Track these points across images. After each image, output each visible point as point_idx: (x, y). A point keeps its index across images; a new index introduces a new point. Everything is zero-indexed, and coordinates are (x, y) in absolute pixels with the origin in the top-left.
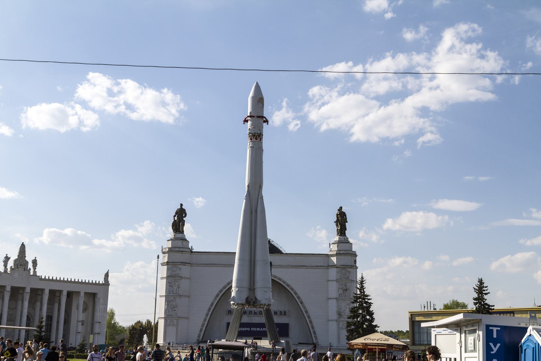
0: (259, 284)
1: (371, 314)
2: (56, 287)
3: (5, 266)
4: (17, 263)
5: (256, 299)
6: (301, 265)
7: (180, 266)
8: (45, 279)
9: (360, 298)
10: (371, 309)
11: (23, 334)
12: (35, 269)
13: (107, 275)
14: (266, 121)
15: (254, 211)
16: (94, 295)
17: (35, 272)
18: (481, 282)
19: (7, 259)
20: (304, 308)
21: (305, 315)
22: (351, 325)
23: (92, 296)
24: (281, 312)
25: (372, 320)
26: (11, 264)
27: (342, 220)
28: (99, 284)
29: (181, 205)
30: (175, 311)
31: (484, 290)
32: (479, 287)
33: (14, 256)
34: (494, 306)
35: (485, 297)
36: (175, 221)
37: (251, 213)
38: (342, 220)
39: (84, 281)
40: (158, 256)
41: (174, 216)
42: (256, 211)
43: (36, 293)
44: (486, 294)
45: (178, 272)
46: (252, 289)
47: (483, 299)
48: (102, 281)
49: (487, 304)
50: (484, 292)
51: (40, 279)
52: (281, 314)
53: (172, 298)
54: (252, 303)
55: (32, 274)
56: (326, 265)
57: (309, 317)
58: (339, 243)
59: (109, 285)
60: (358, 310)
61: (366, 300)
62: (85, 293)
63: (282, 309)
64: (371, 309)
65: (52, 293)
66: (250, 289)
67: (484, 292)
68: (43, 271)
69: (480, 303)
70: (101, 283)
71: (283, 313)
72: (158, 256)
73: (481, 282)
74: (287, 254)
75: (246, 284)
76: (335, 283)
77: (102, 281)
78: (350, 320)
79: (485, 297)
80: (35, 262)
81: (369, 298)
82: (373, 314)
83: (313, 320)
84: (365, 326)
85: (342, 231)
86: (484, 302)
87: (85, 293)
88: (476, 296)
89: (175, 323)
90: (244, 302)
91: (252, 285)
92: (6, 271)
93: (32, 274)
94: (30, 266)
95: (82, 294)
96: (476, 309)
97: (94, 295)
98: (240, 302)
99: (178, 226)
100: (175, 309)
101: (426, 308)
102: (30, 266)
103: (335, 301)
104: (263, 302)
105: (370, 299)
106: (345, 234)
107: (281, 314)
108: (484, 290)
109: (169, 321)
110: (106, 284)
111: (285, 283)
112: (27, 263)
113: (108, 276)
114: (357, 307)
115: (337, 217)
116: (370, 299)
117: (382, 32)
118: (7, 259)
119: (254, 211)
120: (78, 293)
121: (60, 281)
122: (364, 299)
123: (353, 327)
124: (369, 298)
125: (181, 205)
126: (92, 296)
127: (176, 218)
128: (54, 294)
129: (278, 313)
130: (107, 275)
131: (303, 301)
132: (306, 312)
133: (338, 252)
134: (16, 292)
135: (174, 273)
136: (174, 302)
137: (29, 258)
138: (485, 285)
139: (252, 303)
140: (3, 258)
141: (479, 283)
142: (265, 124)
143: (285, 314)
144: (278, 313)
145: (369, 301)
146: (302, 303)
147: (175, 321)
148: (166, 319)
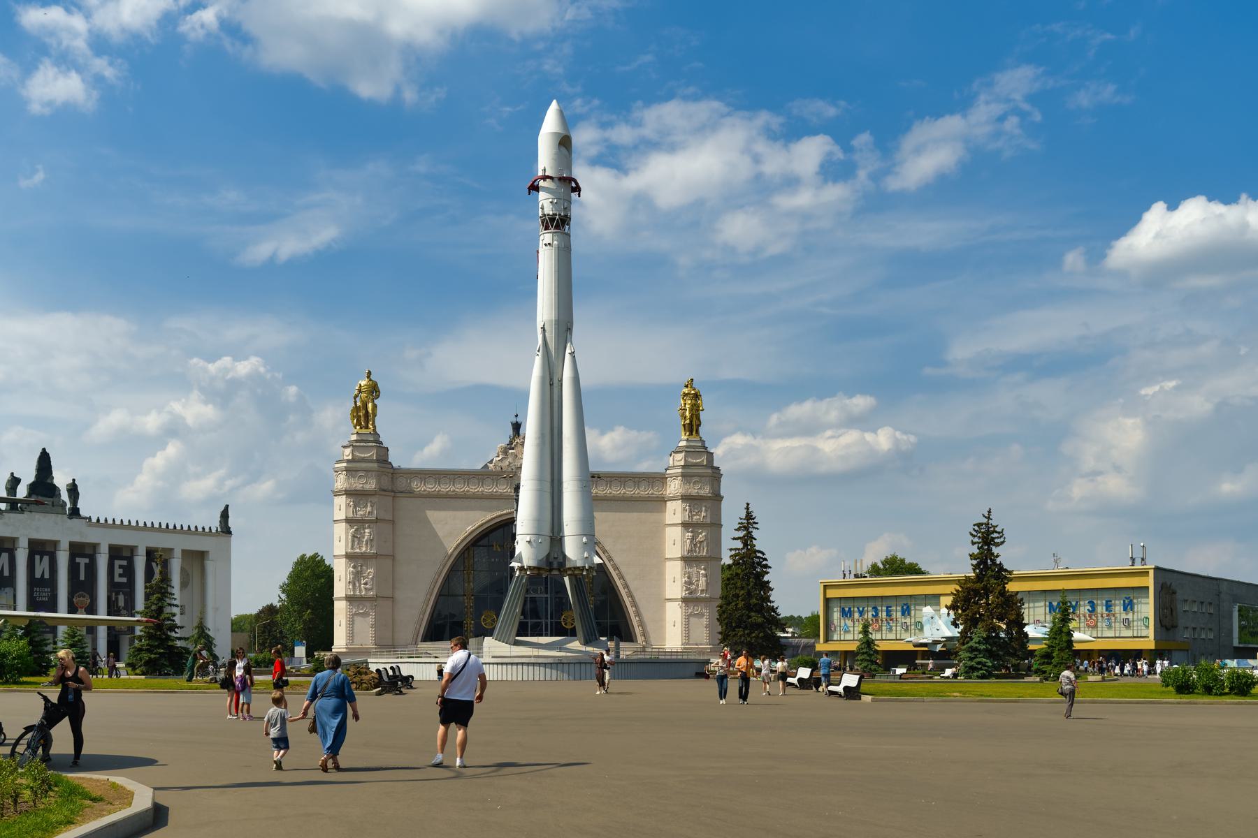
11: (102, 632)
13: (225, 515)
14: (577, 189)
16: (201, 556)
19: (14, 482)
23: (197, 558)
33: (28, 475)
37: (551, 385)
44: (997, 545)
46: (556, 539)
58: (688, 451)
62: (184, 551)
65: (116, 552)
66: (552, 539)
77: (215, 524)
79: (995, 550)
80: (73, 490)
85: (693, 427)
87: (184, 551)
94: (65, 496)
95: (178, 554)
99: (363, 416)
101: (1138, 561)
102: (65, 496)
110: (226, 530)
117: (40, 177)
130: (225, 515)
137: (61, 480)
142: (574, 195)
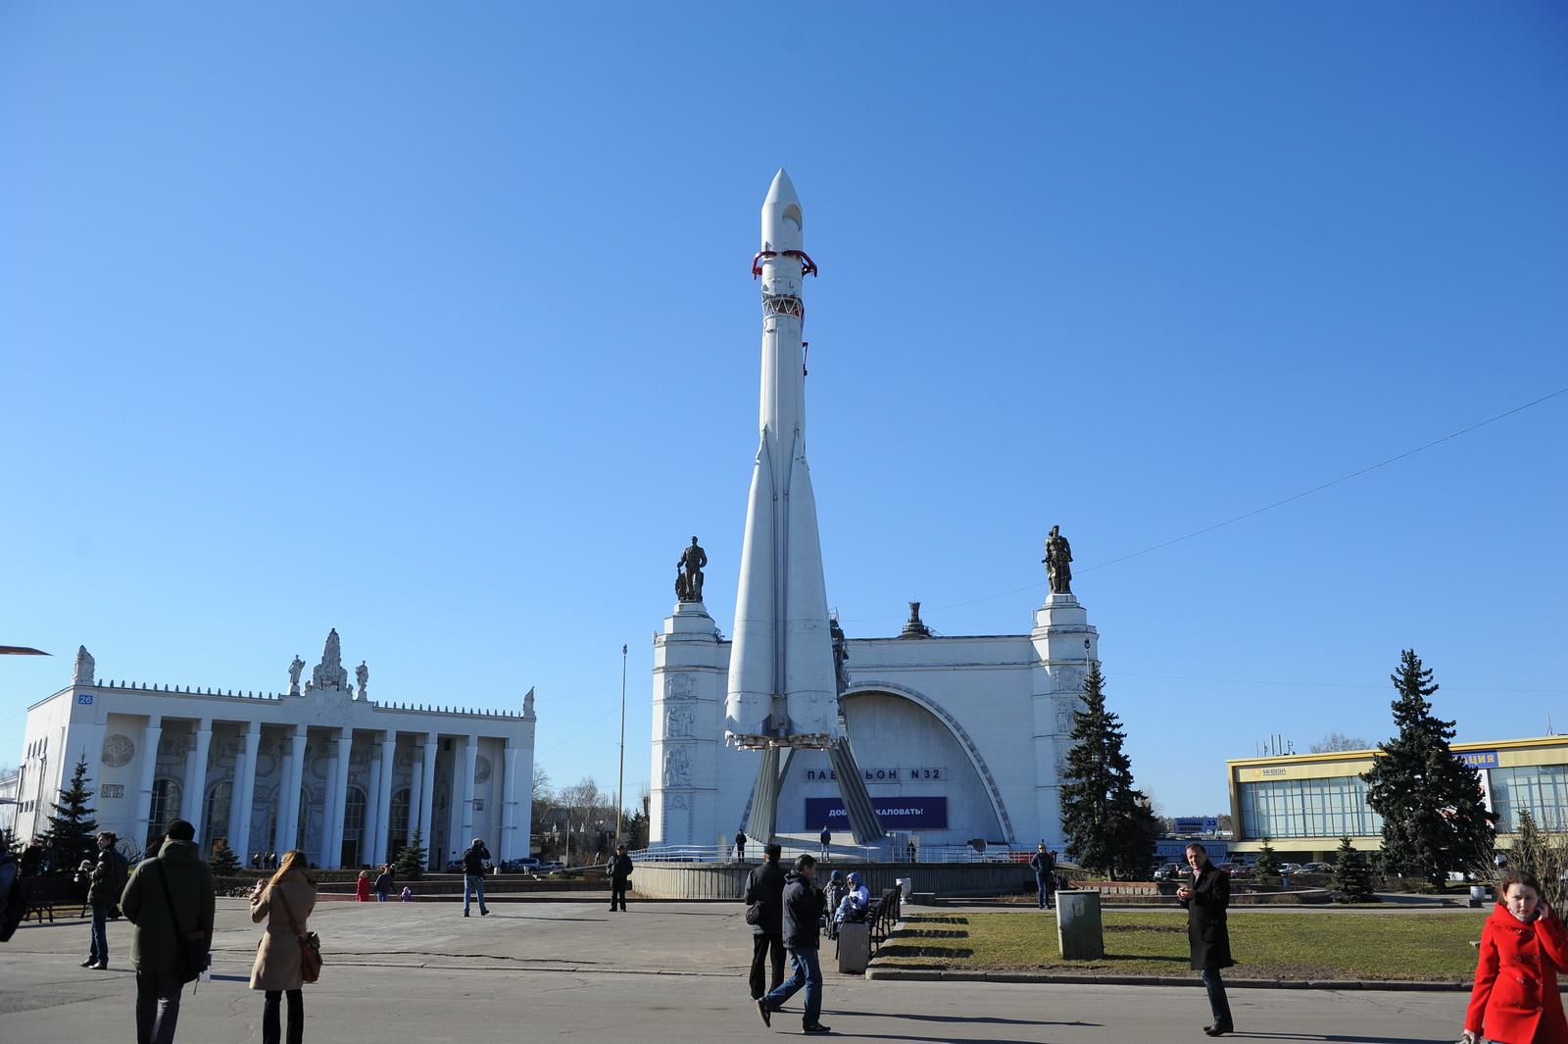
0: (795, 682)
1: (1122, 763)
2: (412, 726)
3: (295, 683)
4: (322, 673)
5: (790, 722)
6: (967, 661)
7: (692, 675)
8: (386, 709)
9: (1092, 724)
10: (1122, 752)
12: (363, 686)
15: (780, 495)
16: (502, 743)
17: (362, 692)
18: (1411, 659)
19: (298, 665)
20: (980, 760)
21: (982, 776)
22: (1072, 793)
23: (498, 744)
24: (927, 772)
25: (1127, 779)
26: (307, 676)
27: (1059, 556)
28: (512, 718)
29: (695, 540)
30: (684, 774)
31: (1423, 684)
32: (1406, 674)
33: (314, 658)
34: (1453, 723)
35: (1426, 699)
36: (681, 576)
38: (1059, 556)
39: (442, 710)
40: (625, 647)
41: (680, 565)
42: (786, 494)
43: (367, 742)
44: (1427, 692)
45: (689, 687)
47: (1422, 707)
48: (518, 710)
49: (1432, 721)
50: (1421, 688)
51: (375, 707)
52: (928, 777)
53: (678, 747)
54: (782, 734)
55: (355, 696)
56: (1025, 660)
57: (991, 781)
59: (534, 719)
60: (1089, 754)
61: (1109, 729)
63: (931, 763)
64: (1122, 752)
67: (1421, 688)
68: (383, 691)
69: (1415, 721)
70: (516, 715)
71: (932, 775)
72: (625, 647)
73: (1411, 659)
74: (942, 638)
75: (764, 684)
76: (1048, 699)
77: (518, 710)
78: (1070, 782)
79: (1426, 699)
80: (362, 673)
81: (1114, 722)
82: (1127, 764)
83: (1001, 790)
84: (1109, 795)
86: (1423, 714)
87: (479, 738)
88: (1399, 698)
89: (686, 803)
90: (759, 730)
91: (781, 686)
92: (295, 693)
93: (355, 696)
95: (473, 740)
96: (1403, 735)
97: (501, 742)
98: (746, 732)
100: (685, 770)
102: (352, 679)
103: (1049, 742)
104: (808, 731)
105: (1118, 726)
106: (1067, 589)
107: (928, 777)
108: (1423, 684)
109: (671, 797)
110: (530, 717)
111: (931, 704)
112: (345, 672)
113: (533, 700)
114: (1084, 748)
115: (1049, 551)
116: (1118, 726)
118: (298, 665)
119: (780, 495)
120: (465, 738)
121: (395, 710)
122: (1103, 727)
123: (1076, 799)
124: (1114, 722)
125: (695, 540)
126: (498, 744)
127: (684, 569)
128: (409, 743)
129: (922, 774)
130: (530, 698)
131: (977, 745)
132: (985, 769)
133: (1053, 629)
134: (322, 739)
135: (681, 690)
136: (683, 754)
137: (349, 663)
138: (1423, 669)
139: (782, 734)
140: (289, 665)
141: (1406, 665)
143: (935, 777)
144: (922, 774)
145: (1116, 731)
146: (973, 749)
147: (686, 797)
148: (666, 792)
